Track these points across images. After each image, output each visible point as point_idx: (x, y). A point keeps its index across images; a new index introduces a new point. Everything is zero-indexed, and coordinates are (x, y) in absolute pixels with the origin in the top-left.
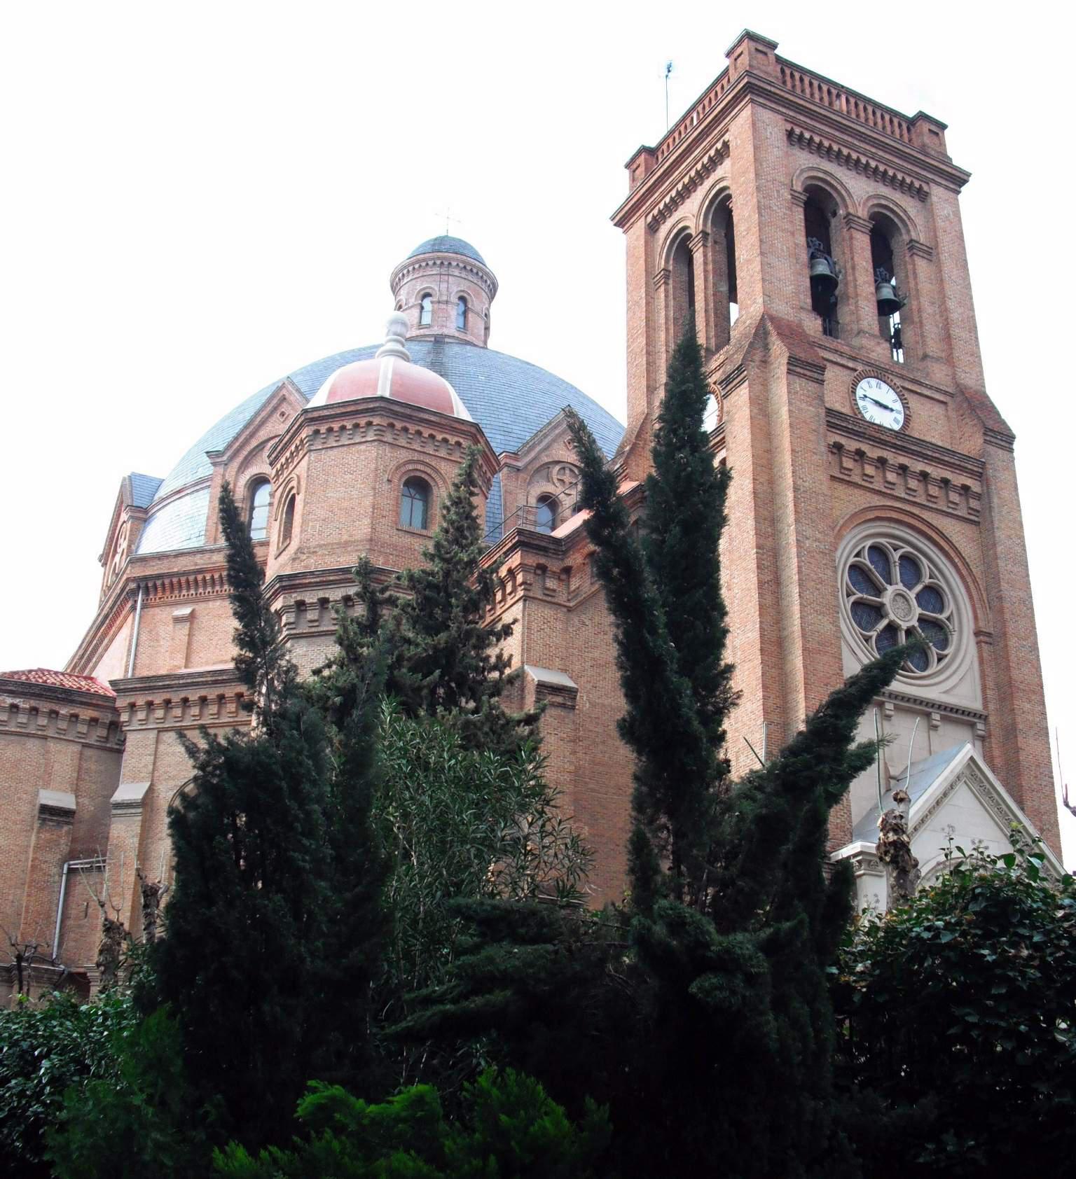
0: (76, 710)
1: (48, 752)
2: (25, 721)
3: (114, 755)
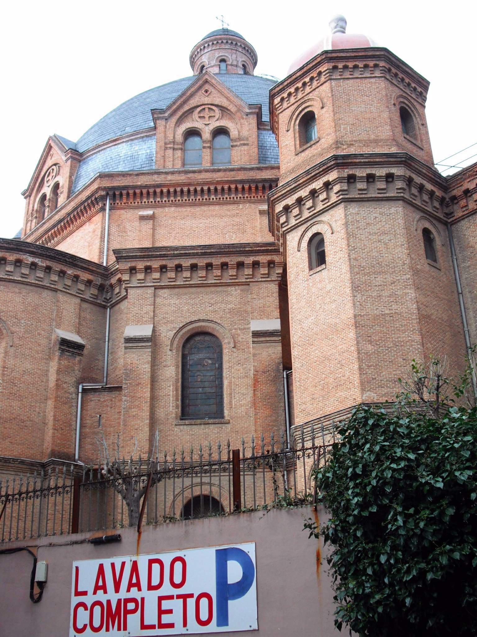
0: (78, 272)
1: (58, 301)
2: (42, 276)
3: (102, 309)
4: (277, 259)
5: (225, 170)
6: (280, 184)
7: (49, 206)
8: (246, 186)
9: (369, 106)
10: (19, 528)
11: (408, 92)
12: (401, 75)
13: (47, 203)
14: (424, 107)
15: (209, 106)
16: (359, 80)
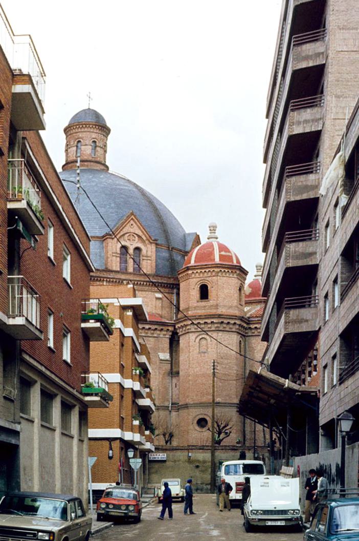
10: (352, 495)
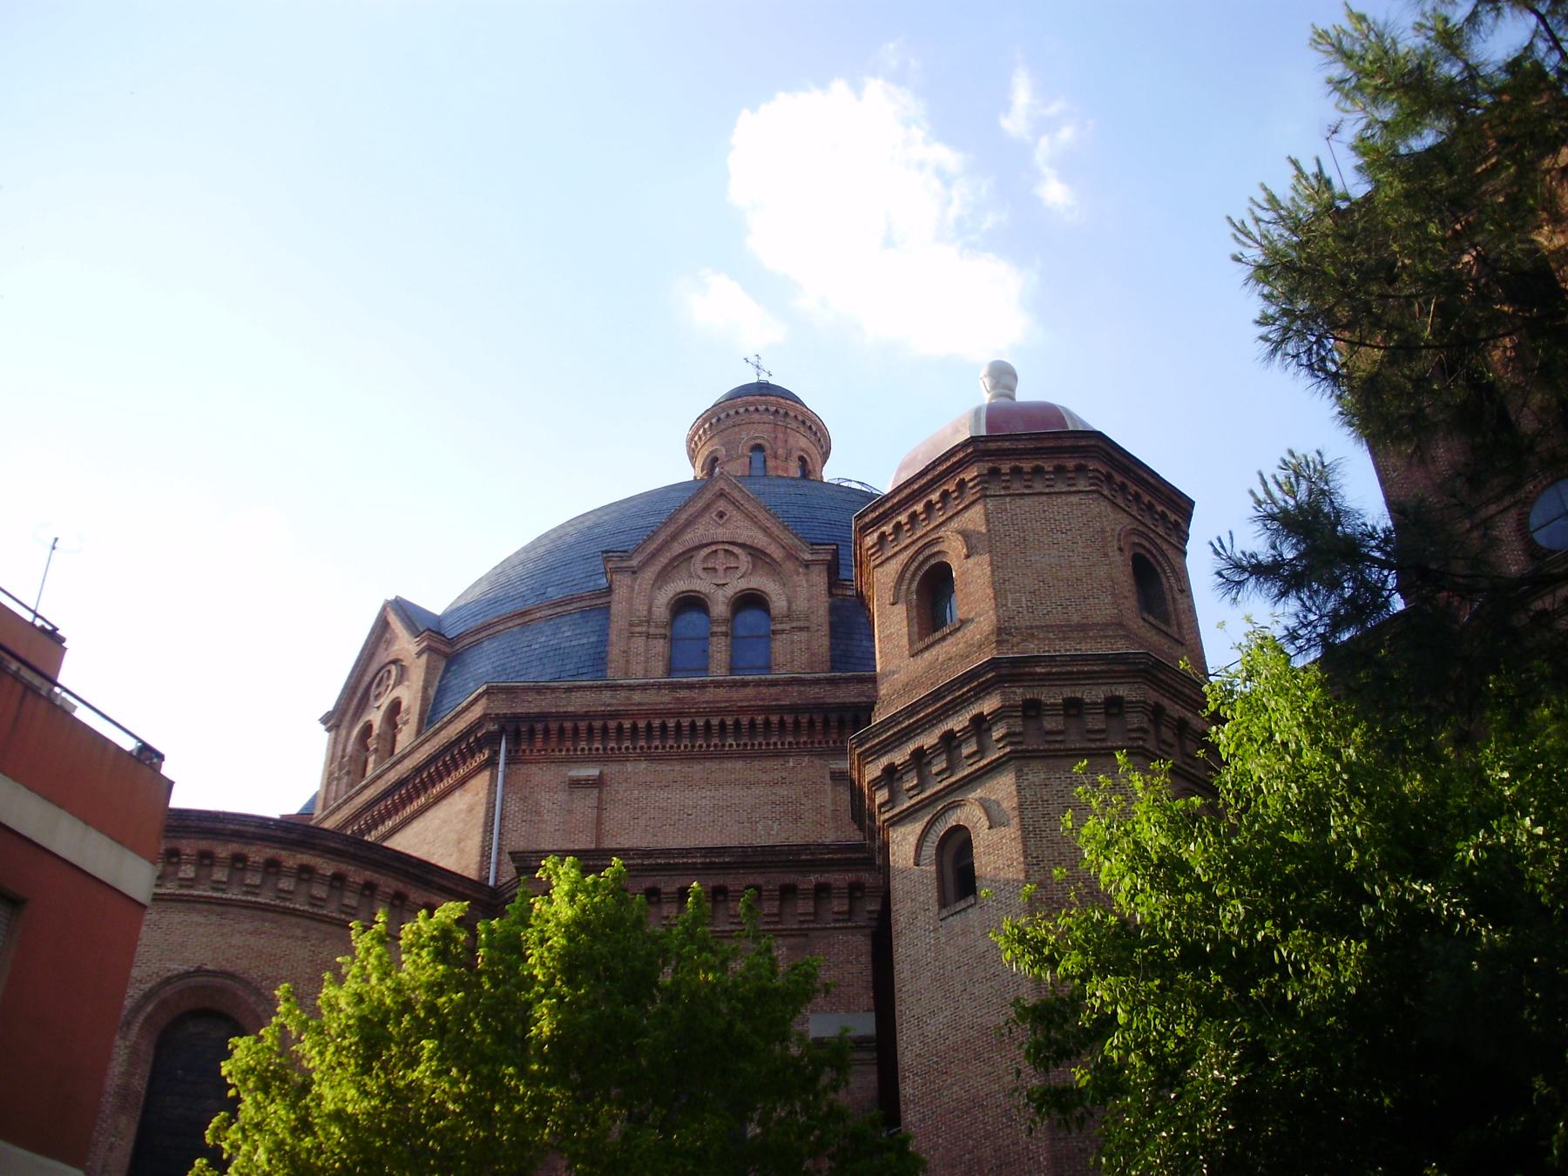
2: (354, 903)
4: (867, 878)
5: (758, 684)
6: (877, 719)
7: (376, 750)
8: (804, 720)
9: (1066, 553)
11: (1149, 523)
12: (1133, 488)
13: (372, 743)
14: (1185, 554)
15: (727, 547)
16: (1044, 498)
